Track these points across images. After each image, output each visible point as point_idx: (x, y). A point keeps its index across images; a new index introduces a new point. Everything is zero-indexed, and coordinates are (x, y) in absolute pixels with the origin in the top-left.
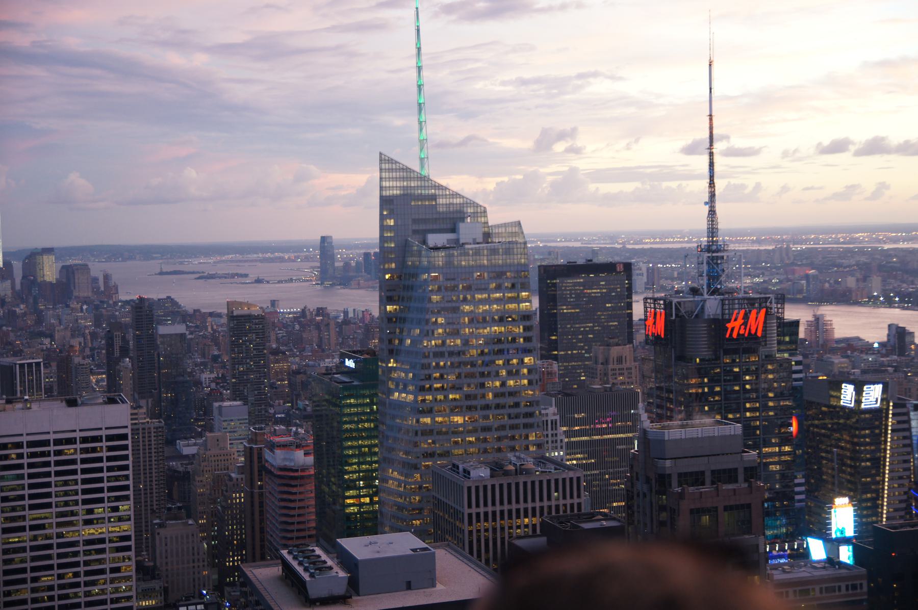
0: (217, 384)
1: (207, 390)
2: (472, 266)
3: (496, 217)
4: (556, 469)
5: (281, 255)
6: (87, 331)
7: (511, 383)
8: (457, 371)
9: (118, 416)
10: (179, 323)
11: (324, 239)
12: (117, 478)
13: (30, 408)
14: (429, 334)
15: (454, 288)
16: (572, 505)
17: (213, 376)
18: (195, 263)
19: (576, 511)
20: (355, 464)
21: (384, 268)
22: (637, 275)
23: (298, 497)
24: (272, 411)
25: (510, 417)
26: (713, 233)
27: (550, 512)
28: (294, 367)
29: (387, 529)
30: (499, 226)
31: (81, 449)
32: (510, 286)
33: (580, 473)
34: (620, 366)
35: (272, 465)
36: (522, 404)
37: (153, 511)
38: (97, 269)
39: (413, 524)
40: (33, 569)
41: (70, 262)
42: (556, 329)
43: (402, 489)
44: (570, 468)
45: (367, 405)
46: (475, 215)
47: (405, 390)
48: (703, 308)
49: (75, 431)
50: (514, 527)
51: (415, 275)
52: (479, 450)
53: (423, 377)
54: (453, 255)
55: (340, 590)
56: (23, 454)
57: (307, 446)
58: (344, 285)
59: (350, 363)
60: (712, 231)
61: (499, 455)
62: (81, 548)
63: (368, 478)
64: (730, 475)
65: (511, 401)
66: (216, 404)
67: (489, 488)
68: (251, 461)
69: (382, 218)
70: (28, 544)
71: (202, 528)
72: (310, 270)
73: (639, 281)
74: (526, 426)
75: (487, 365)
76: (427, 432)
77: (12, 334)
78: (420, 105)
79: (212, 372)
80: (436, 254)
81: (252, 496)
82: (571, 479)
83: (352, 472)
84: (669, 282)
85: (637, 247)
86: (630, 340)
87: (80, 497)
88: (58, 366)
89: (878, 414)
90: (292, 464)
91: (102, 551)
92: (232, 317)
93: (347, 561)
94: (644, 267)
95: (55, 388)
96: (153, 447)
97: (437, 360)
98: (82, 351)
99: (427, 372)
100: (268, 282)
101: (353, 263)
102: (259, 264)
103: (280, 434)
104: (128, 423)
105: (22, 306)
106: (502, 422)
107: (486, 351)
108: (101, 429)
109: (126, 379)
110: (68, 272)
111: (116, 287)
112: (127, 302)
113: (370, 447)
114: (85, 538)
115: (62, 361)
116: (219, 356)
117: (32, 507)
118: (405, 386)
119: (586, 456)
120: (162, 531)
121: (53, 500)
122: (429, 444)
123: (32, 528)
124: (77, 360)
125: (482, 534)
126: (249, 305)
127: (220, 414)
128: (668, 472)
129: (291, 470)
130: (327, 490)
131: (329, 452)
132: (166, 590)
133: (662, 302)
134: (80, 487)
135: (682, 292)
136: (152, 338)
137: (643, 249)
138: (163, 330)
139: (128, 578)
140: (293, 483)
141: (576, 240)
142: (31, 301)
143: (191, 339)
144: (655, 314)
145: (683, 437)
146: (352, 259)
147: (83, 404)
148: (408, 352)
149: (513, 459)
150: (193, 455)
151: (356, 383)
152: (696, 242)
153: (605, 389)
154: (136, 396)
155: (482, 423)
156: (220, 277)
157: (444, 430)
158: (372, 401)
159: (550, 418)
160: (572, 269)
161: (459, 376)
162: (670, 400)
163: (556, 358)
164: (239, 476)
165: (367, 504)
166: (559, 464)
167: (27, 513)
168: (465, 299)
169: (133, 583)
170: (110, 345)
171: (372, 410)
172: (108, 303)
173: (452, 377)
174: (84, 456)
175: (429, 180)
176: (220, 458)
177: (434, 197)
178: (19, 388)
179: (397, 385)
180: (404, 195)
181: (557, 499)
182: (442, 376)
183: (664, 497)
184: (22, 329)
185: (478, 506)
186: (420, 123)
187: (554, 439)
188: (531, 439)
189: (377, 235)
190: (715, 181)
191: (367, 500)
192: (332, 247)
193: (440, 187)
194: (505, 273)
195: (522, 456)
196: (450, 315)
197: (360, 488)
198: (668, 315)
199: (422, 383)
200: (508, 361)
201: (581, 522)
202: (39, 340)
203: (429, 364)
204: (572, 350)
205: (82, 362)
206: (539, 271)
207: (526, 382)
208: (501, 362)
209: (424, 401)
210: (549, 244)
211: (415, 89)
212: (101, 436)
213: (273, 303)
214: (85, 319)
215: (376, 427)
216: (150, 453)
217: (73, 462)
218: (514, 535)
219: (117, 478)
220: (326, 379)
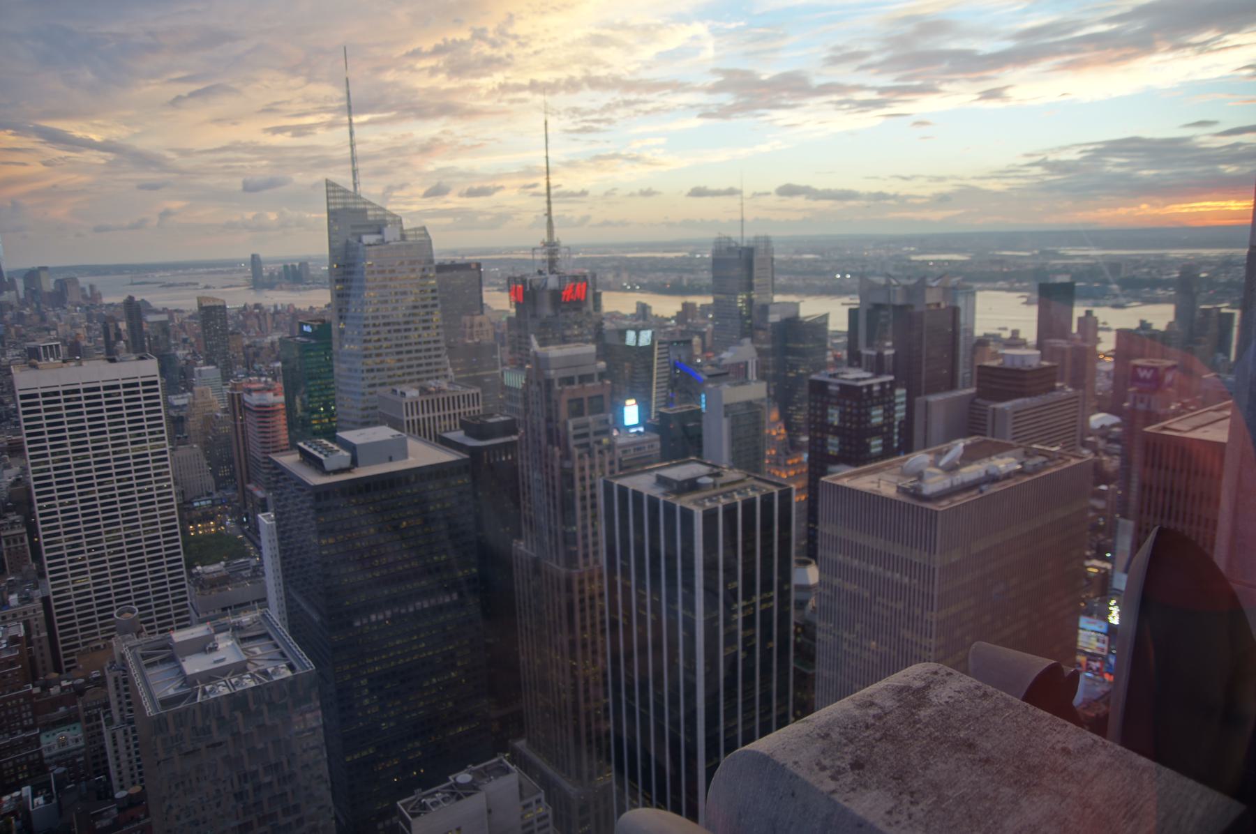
11: (253, 256)
18: (167, 276)
38: (84, 281)
41: (61, 277)
46: (394, 222)
55: (347, 464)
64: (584, 379)
81: (236, 426)
89: (649, 350)
126: (214, 299)
170: (107, 335)
177: (364, 211)
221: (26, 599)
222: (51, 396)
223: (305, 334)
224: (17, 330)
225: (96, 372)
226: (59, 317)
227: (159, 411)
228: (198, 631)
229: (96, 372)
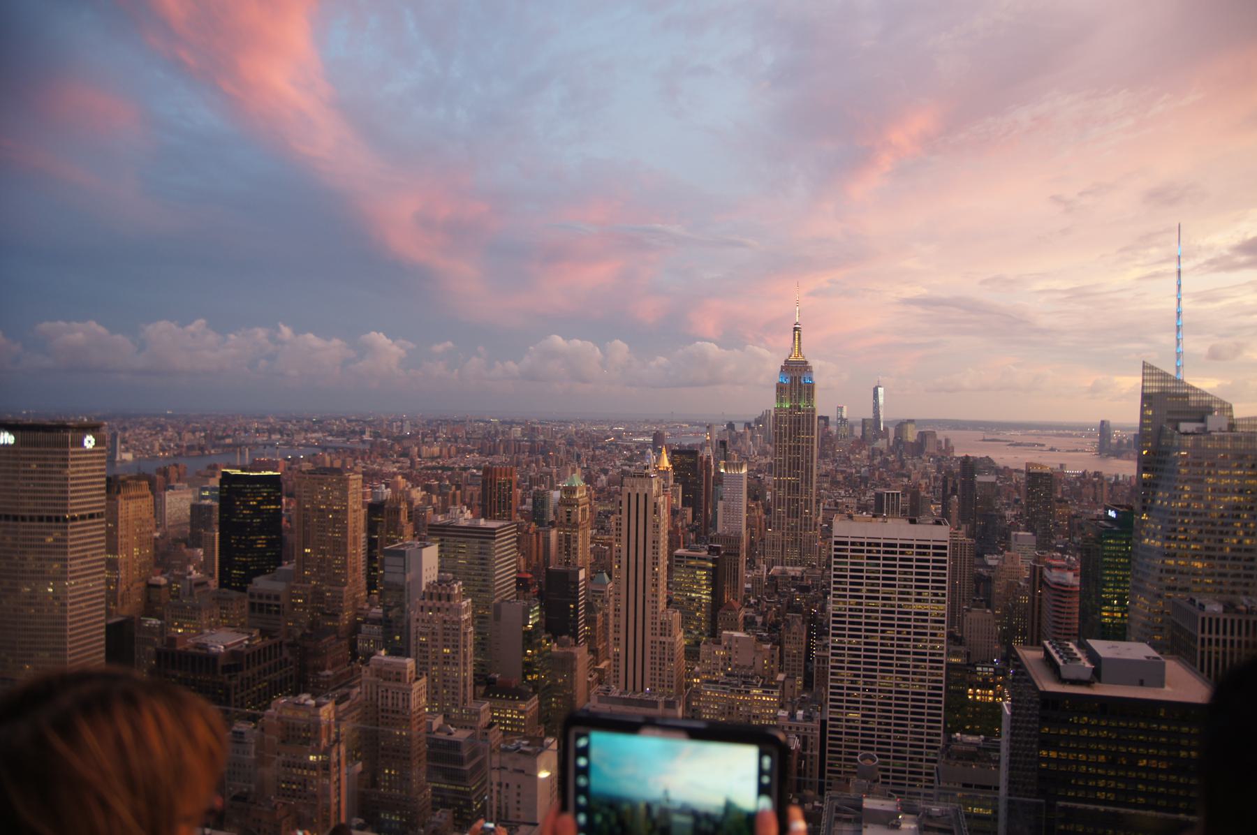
7: (1248, 541)
9: (942, 534)
11: (1103, 422)
12: (938, 575)
14: (1176, 498)
15: (1200, 465)
18: (1017, 435)
30: (1242, 419)
38: (941, 435)
40: (883, 625)
46: (1222, 410)
51: (1168, 453)
55: (1086, 676)
61: (1233, 597)
62: (912, 617)
65: (1247, 555)
69: (1142, 409)
71: (997, 616)
72: (1091, 443)
76: (1170, 571)
81: (1034, 599)
87: (914, 583)
91: (926, 621)
92: (1029, 474)
93: (1093, 656)
98: (927, 487)
99: (1173, 526)
104: (948, 539)
110: (923, 435)
112: (958, 458)
113: (1124, 576)
117: (884, 585)
118: (1154, 535)
120: (969, 615)
121: (897, 583)
123: (883, 598)
124: (923, 494)
126: (1042, 466)
129: (1062, 585)
131: (1091, 575)
132: (968, 654)
136: (972, 484)
139: (941, 642)
148: (1158, 510)
149: (1245, 601)
155: (1218, 570)
161: (1201, 532)
167: (880, 588)
169: (944, 645)
170: (945, 486)
175: (1183, 382)
177: (1187, 395)
179: (1148, 534)
182: (1185, 530)
193: (1192, 388)
213: (1062, 466)
217: (911, 560)
219: (938, 575)
220: (1093, 523)
221: (808, 718)
222: (857, 546)
224: (881, 473)
225: (895, 529)
226: (915, 466)
227: (944, 575)
228: (888, 805)
229: (895, 529)
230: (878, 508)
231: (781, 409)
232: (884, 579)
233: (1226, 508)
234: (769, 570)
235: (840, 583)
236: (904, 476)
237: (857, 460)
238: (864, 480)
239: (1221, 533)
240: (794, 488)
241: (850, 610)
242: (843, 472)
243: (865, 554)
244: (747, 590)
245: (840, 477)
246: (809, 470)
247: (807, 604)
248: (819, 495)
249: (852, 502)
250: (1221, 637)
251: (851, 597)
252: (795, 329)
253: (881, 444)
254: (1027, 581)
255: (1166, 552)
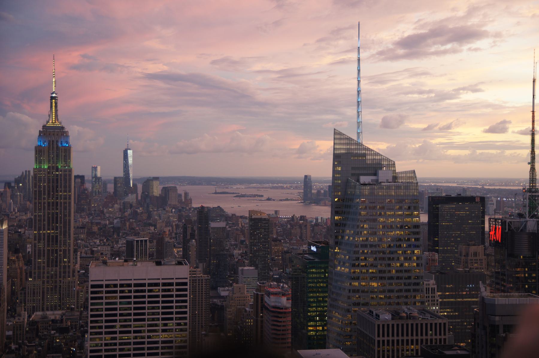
0: (242, 256)
1: (236, 260)
2: (385, 196)
3: (401, 167)
4: (431, 317)
5: (282, 185)
6: (174, 224)
8: (374, 256)
9: (182, 272)
10: (223, 221)
11: (306, 176)
12: (181, 307)
13: (136, 265)
14: (359, 234)
15: (374, 208)
16: (440, 340)
17: (240, 252)
18: (242, 189)
19: (443, 343)
20: (314, 307)
21: (334, 195)
22: (490, 204)
23: (282, 324)
24: (271, 273)
25: (405, 284)
26: (533, 181)
27: (427, 343)
28: (285, 249)
29: (331, 346)
30: (402, 173)
31: (162, 289)
32: (407, 208)
33: (446, 321)
34: (475, 258)
35: (268, 305)
36: (412, 278)
37: (202, 326)
38: (181, 189)
39: (346, 344)
42: (438, 234)
43: (340, 323)
44: (440, 317)
45: (322, 272)
46: (388, 166)
47: (344, 265)
48: (525, 226)
49: (159, 279)
50: (405, 350)
51: (352, 200)
52: (386, 303)
53: (355, 259)
54: (374, 189)
56: (131, 290)
57: (288, 295)
58: (317, 203)
59: (314, 249)
60: (533, 179)
62: (160, 345)
63: (322, 316)
65: (406, 275)
66: (240, 268)
67: (391, 326)
68: (257, 302)
69: (334, 166)
70: (132, 341)
72: (297, 193)
73: (491, 207)
74: (415, 290)
75: (392, 253)
77: (134, 223)
78: (358, 102)
79: (239, 250)
80: (364, 187)
82: (440, 324)
83: (313, 312)
84: (510, 209)
85: (491, 187)
86: (483, 243)
88: (157, 242)
90: (280, 305)
92: (251, 219)
94: (494, 200)
95: (155, 254)
96: (204, 290)
97: (363, 249)
98: (170, 234)
99: (357, 256)
100: (274, 200)
101: (322, 192)
102: (269, 190)
103: (273, 286)
104: (188, 276)
105: (141, 209)
106: (400, 288)
107: (392, 245)
108: (173, 279)
109: (193, 253)
110: (166, 190)
111: (191, 200)
114: (162, 339)
115: (159, 239)
116: (244, 241)
117: (135, 320)
118: (344, 263)
119: (453, 310)
121: (146, 317)
122: (357, 298)
123: (135, 332)
124: (167, 239)
125: (386, 353)
126: (261, 213)
127: (242, 274)
128: (497, 324)
130: (298, 321)
131: (299, 298)
133: (500, 221)
134: (161, 311)
135: (513, 216)
137: (494, 189)
138: (213, 225)
140: (280, 316)
141: (454, 182)
142: (146, 206)
143: (230, 231)
144: (496, 228)
145: (507, 303)
146: (322, 189)
147: (164, 264)
149: (406, 310)
150: (226, 296)
151: (316, 260)
152: (522, 186)
153: (466, 271)
154: (197, 261)
155: (388, 287)
156: (248, 197)
157: (366, 290)
158: (325, 271)
159: (431, 287)
160: (448, 200)
161: (375, 259)
162: (504, 280)
163: (437, 251)
164: (251, 310)
165: (321, 331)
166: (433, 314)
167: (132, 323)
168: (380, 214)
170: (185, 232)
171: (325, 276)
172: (186, 208)
173: (371, 260)
174: (164, 293)
175: (362, 145)
176: (240, 299)
177: (364, 155)
178: (135, 254)
179: (339, 263)
180: (347, 153)
181: (431, 335)
182: (365, 259)
183: (494, 339)
184: (140, 221)
185: (383, 336)
186: (358, 112)
187: (433, 299)
188: (417, 298)
189: (331, 176)
190: (535, 150)
191: (321, 328)
192: (311, 181)
193: (368, 149)
194: (404, 200)
195: (411, 308)
196: (372, 223)
197: (317, 321)
198: (503, 229)
199: (354, 262)
200: (405, 252)
201: (444, 350)
202: (148, 228)
203: (358, 251)
204: (447, 247)
205: (170, 241)
206: (429, 199)
207: (415, 264)
208: (400, 252)
209: (354, 272)
210: (437, 184)
211: (356, 92)
212: (173, 283)
214: (173, 217)
215: (327, 286)
216: (202, 294)
217: (157, 296)
218: (405, 355)
219: (181, 307)
222: (111, 288)
223: (312, 253)
224: (131, 224)
225: (144, 271)
229: (144, 271)
230: (129, 254)
231: (40, 170)
232: (115, 315)
233: (392, 241)
234: (29, 317)
235: (96, 322)
236: (151, 225)
237: (110, 213)
238: (117, 230)
239: (389, 259)
240: (53, 240)
241: (106, 345)
242: (97, 224)
243: (119, 295)
244: (8, 337)
245: (95, 229)
246: (67, 224)
247: (66, 344)
248: (76, 245)
249: (107, 250)
250: (400, 338)
251: (106, 333)
252: (52, 98)
253: (131, 198)
254: (251, 306)
255: (353, 275)
